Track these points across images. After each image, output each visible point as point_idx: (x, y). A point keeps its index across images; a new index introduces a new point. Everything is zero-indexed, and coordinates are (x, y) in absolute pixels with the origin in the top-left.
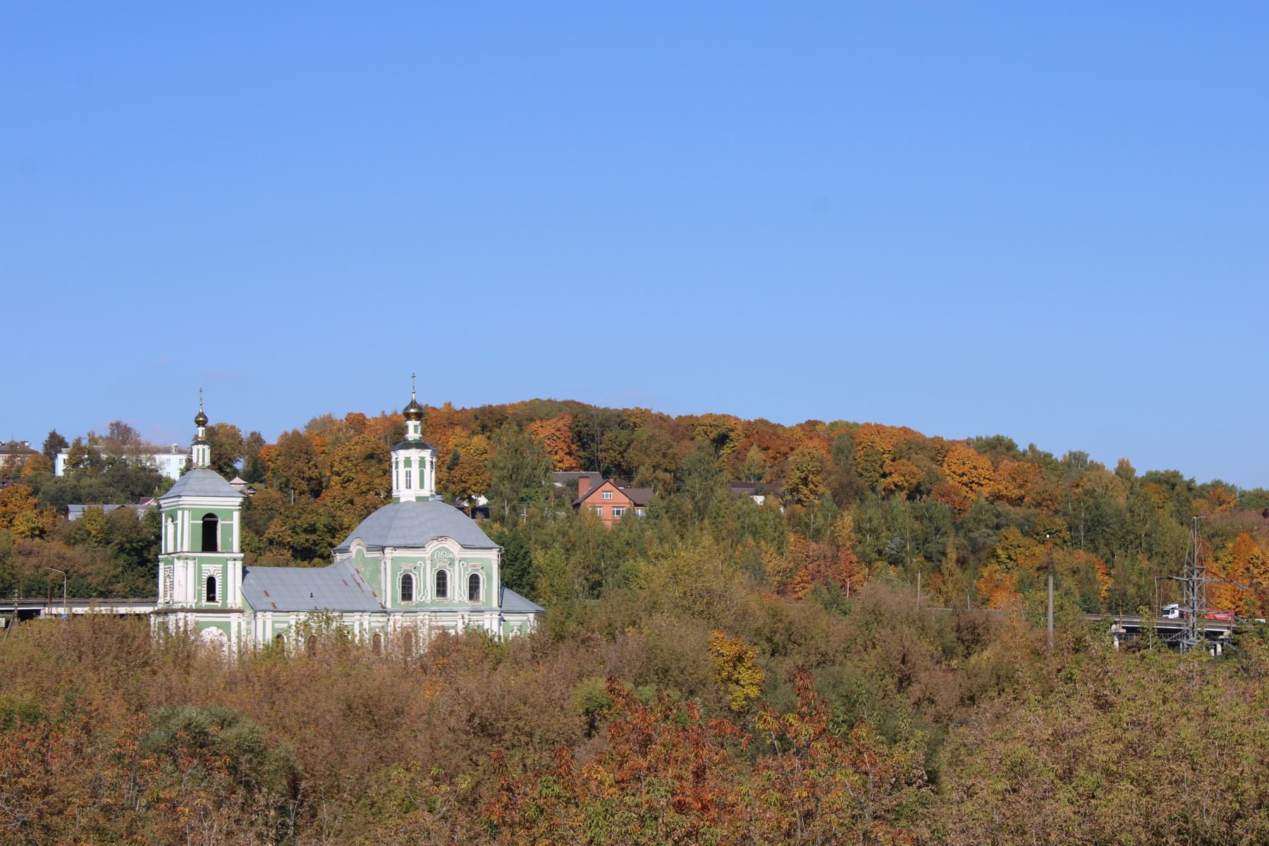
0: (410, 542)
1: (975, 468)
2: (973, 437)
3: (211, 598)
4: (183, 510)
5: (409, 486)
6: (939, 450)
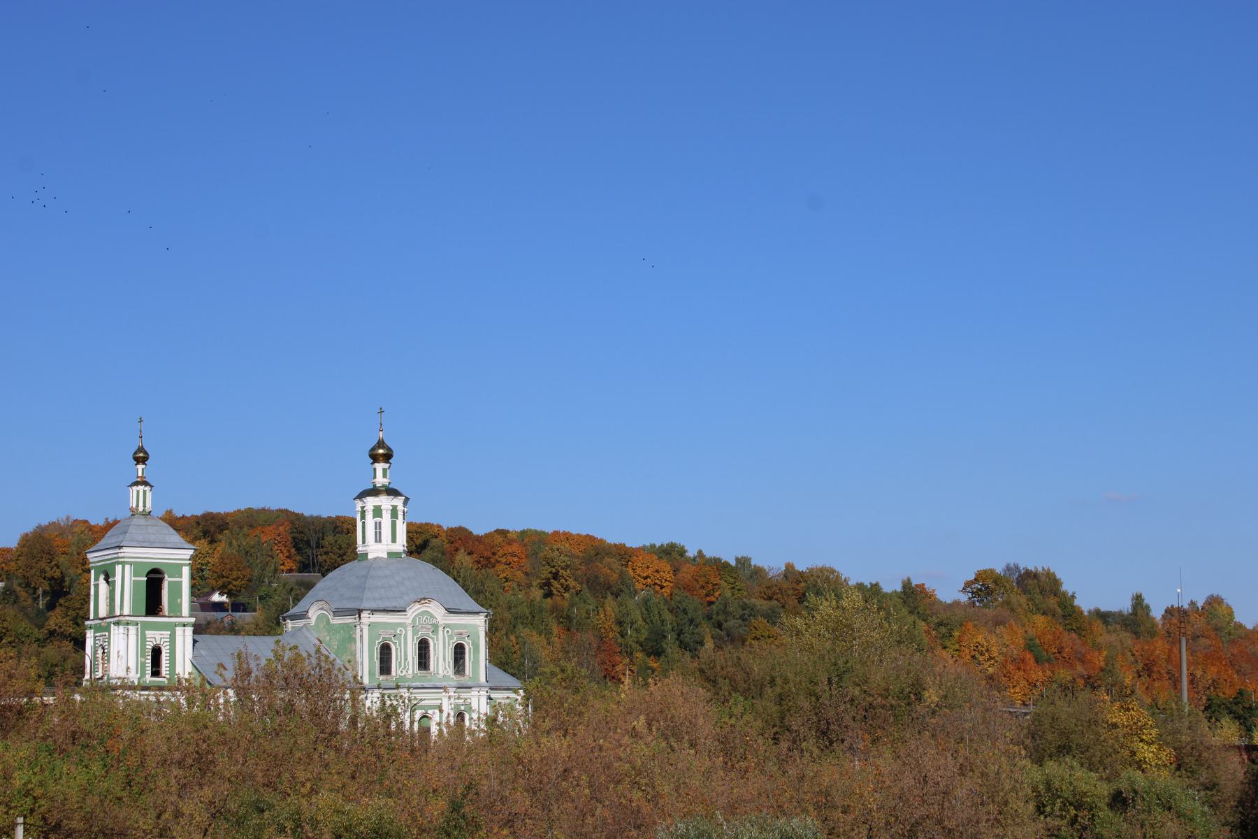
0: (388, 605)
1: (657, 571)
2: (648, 544)
3: (156, 673)
4: (123, 564)
5: (378, 539)
6: (624, 554)
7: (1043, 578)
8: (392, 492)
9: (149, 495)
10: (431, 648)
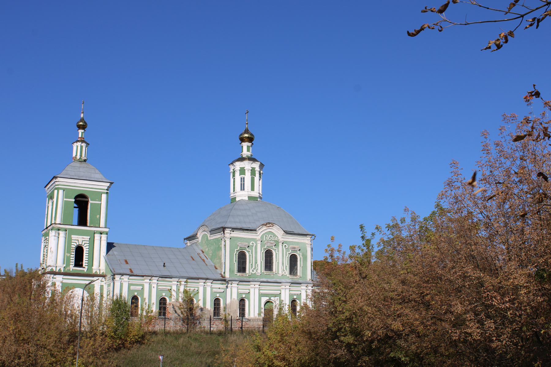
0: (244, 226)
5: (242, 188)
8: (252, 159)
9: (84, 149)
10: (274, 256)
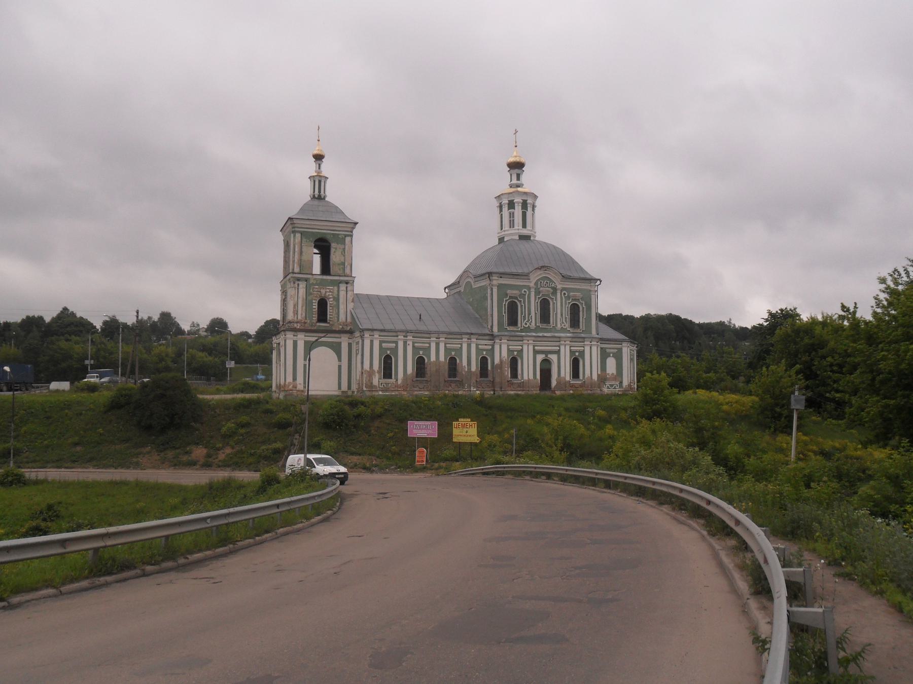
7: (818, 330)
